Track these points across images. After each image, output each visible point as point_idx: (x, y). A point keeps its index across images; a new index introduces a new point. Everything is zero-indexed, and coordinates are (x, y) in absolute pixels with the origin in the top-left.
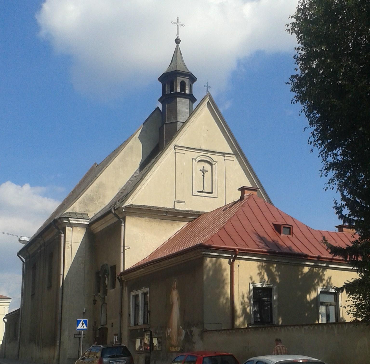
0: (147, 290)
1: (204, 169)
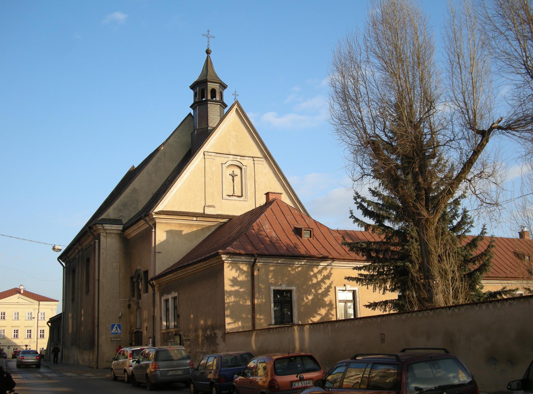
0: (175, 294)
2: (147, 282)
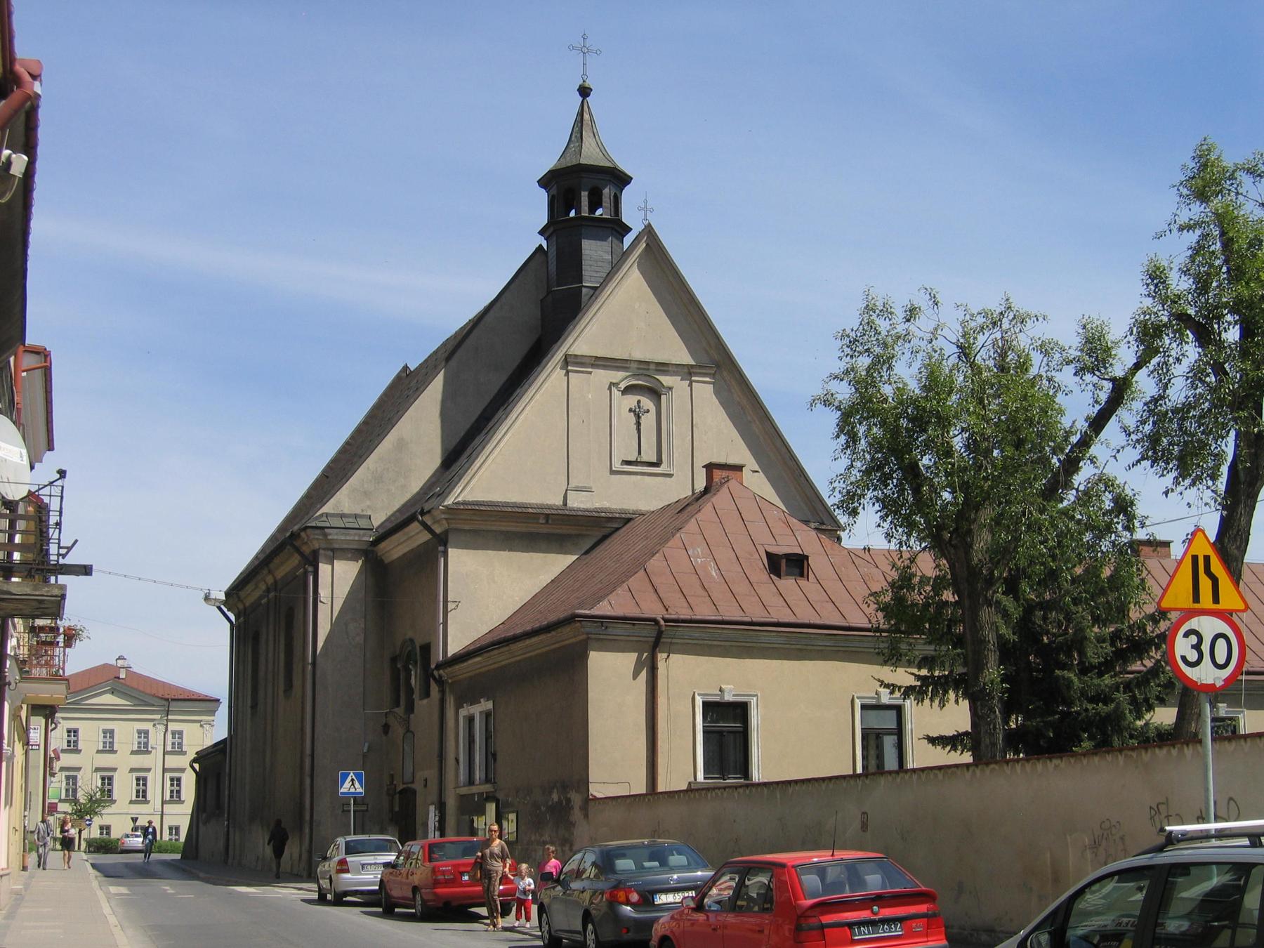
0: (489, 705)
2: (427, 675)
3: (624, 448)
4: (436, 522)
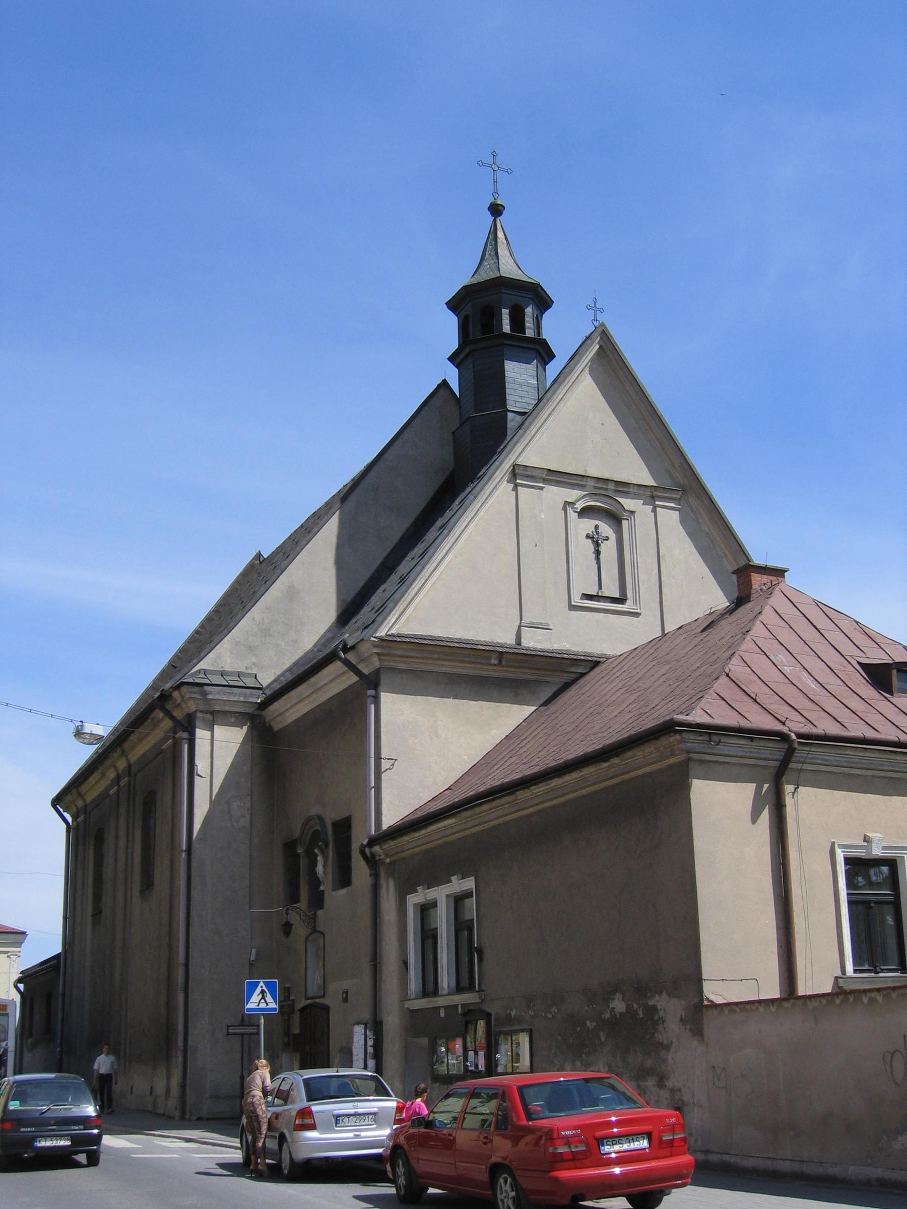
0: (469, 884)
1: (598, 533)
3: (584, 582)
4: (363, 660)
